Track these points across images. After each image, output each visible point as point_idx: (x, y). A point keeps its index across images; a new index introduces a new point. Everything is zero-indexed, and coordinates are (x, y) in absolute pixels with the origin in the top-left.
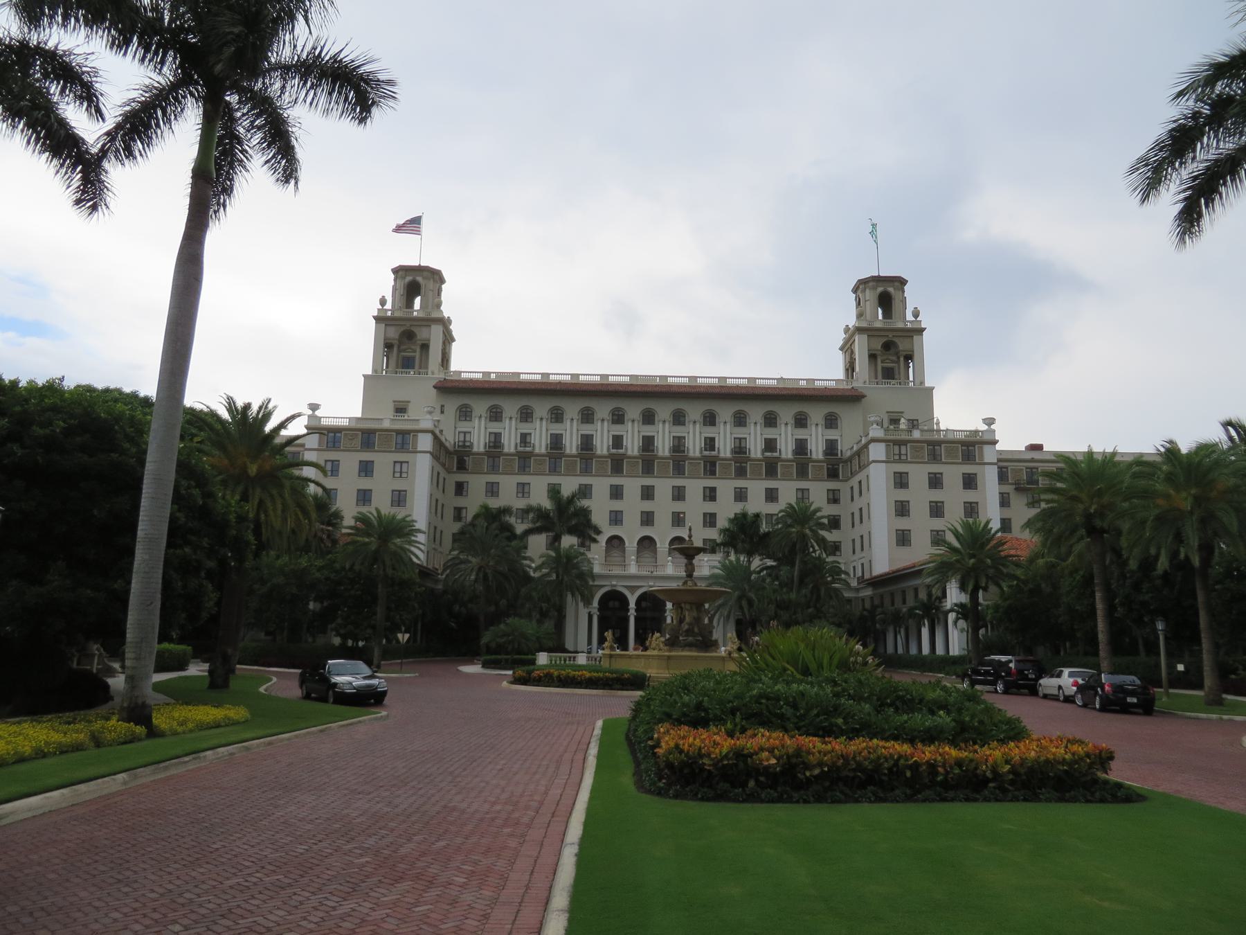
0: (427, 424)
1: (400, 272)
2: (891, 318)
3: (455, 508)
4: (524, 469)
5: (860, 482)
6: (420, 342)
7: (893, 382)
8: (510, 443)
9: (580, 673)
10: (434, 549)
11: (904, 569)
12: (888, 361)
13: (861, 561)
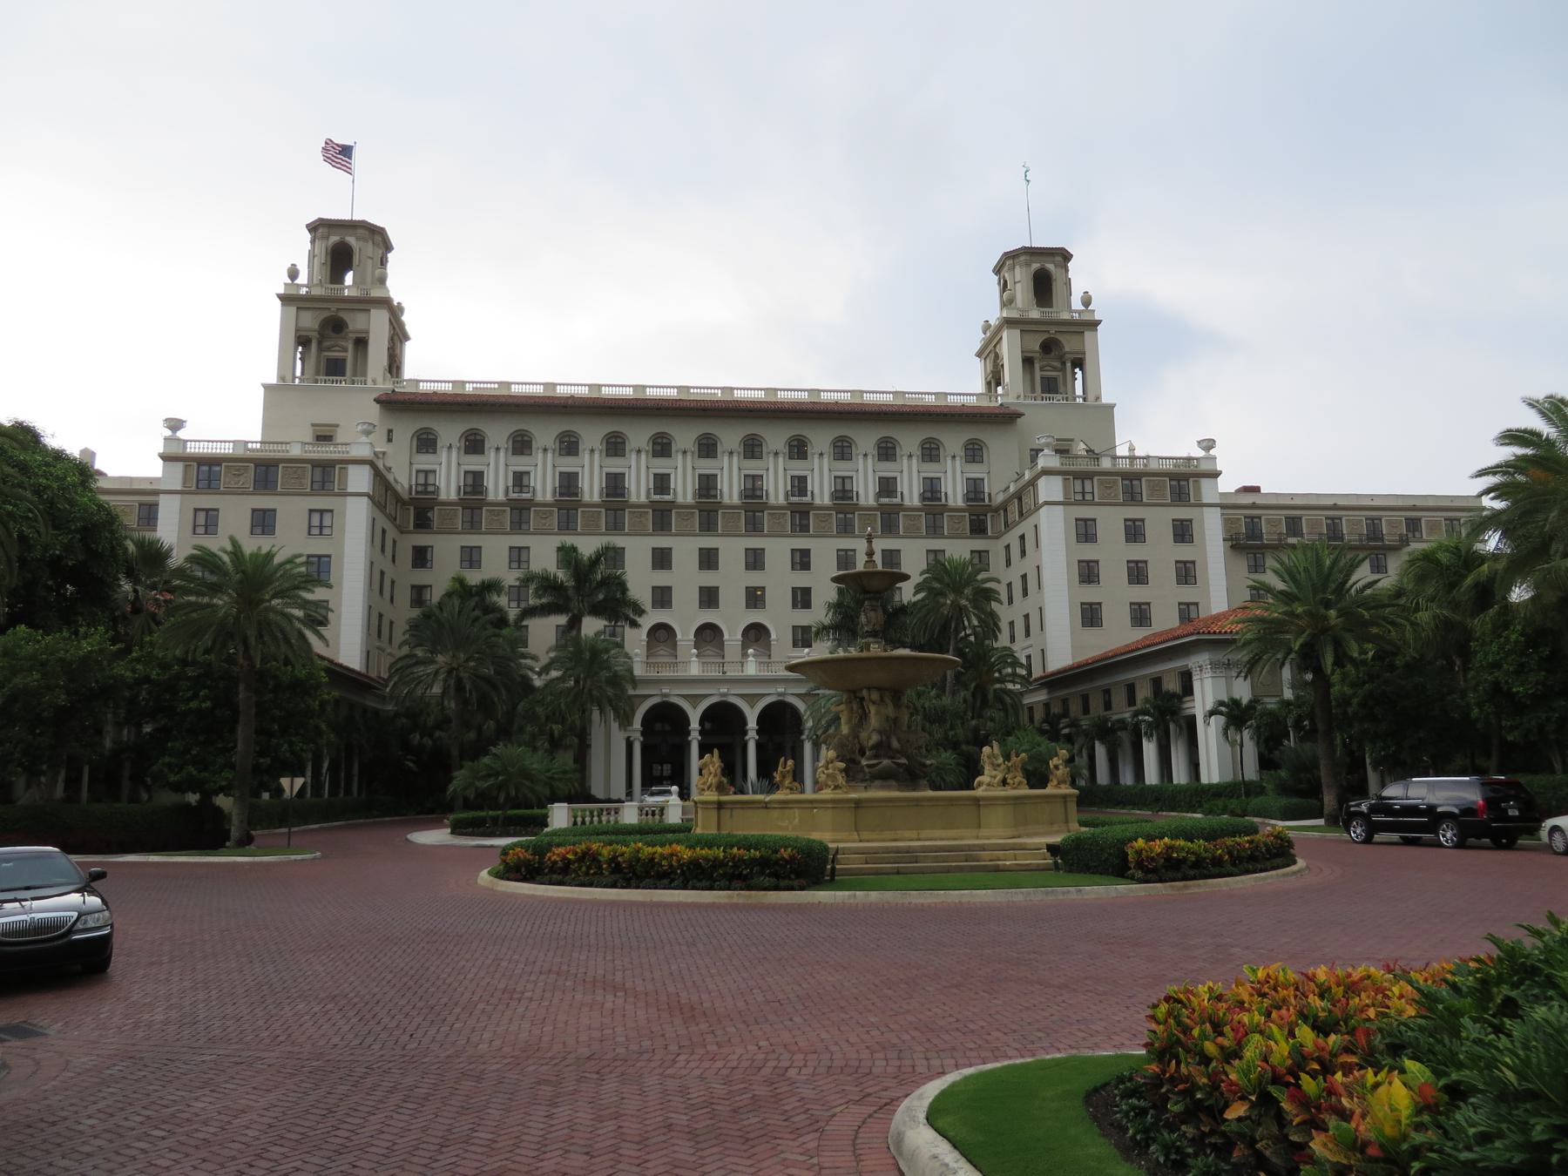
0: (362, 451)
1: (319, 228)
2: (1051, 306)
3: (413, 587)
4: (519, 526)
5: (1022, 537)
6: (353, 336)
7: (1059, 396)
8: (497, 487)
9: (667, 850)
10: (379, 648)
11: (1116, 656)
12: (337, 348)
13: (1027, 652)
